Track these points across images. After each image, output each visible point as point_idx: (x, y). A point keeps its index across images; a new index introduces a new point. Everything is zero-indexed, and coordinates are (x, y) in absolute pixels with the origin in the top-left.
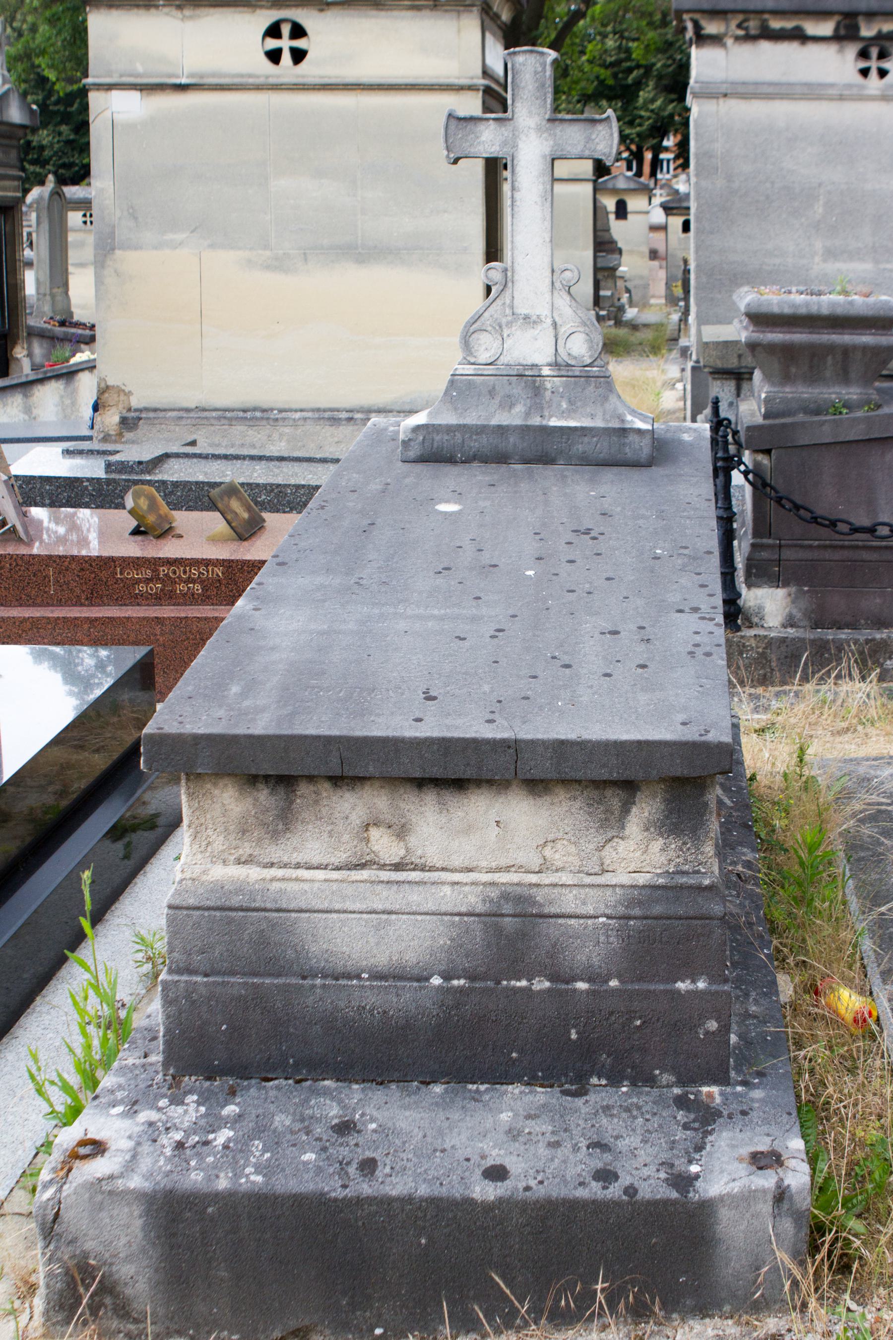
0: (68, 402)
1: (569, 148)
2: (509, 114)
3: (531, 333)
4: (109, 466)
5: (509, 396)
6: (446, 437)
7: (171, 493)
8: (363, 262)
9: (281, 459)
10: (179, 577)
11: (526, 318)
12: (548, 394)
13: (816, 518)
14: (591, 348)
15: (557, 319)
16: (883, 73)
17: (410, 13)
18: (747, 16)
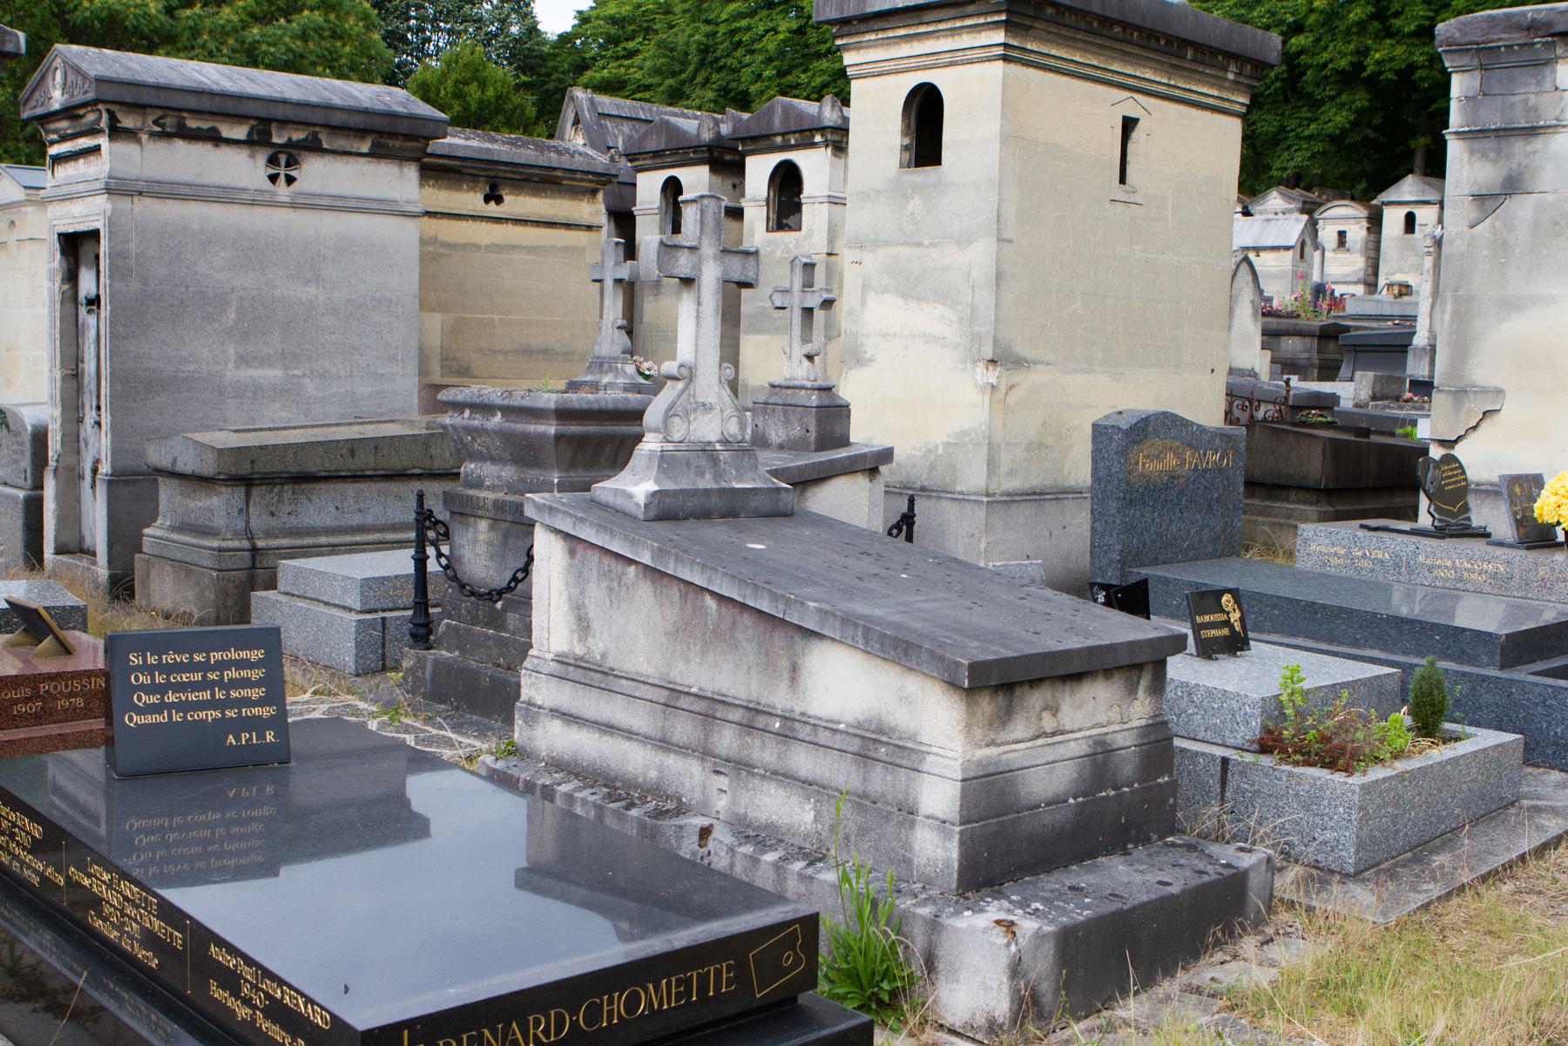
16: (290, 180)
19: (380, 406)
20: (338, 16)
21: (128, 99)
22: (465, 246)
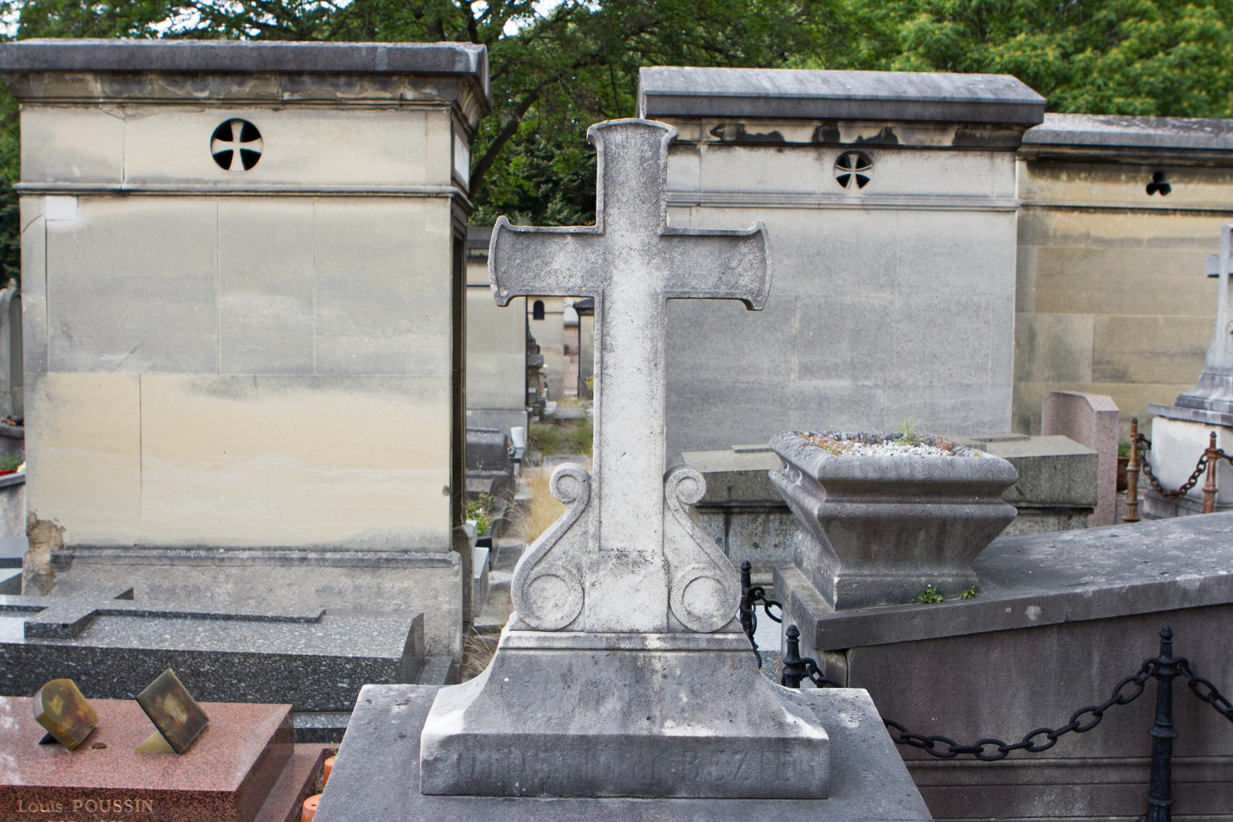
0: (11, 515)
1: (694, 282)
2: (598, 226)
3: (629, 580)
4: (29, 629)
5: (594, 684)
6: (496, 756)
7: (101, 662)
8: (319, 386)
9: (228, 618)
10: (98, 812)
11: (622, 555)
12: (657, 680)
13: (908, 737)
14: (723, 603)
15: (670, 557)
16: (862, 181)
17: (373, 113)
18: (723, 121)
19: (964, 419)
20: (1216, 46)
21: (680, 111)
22: (1122, 242)
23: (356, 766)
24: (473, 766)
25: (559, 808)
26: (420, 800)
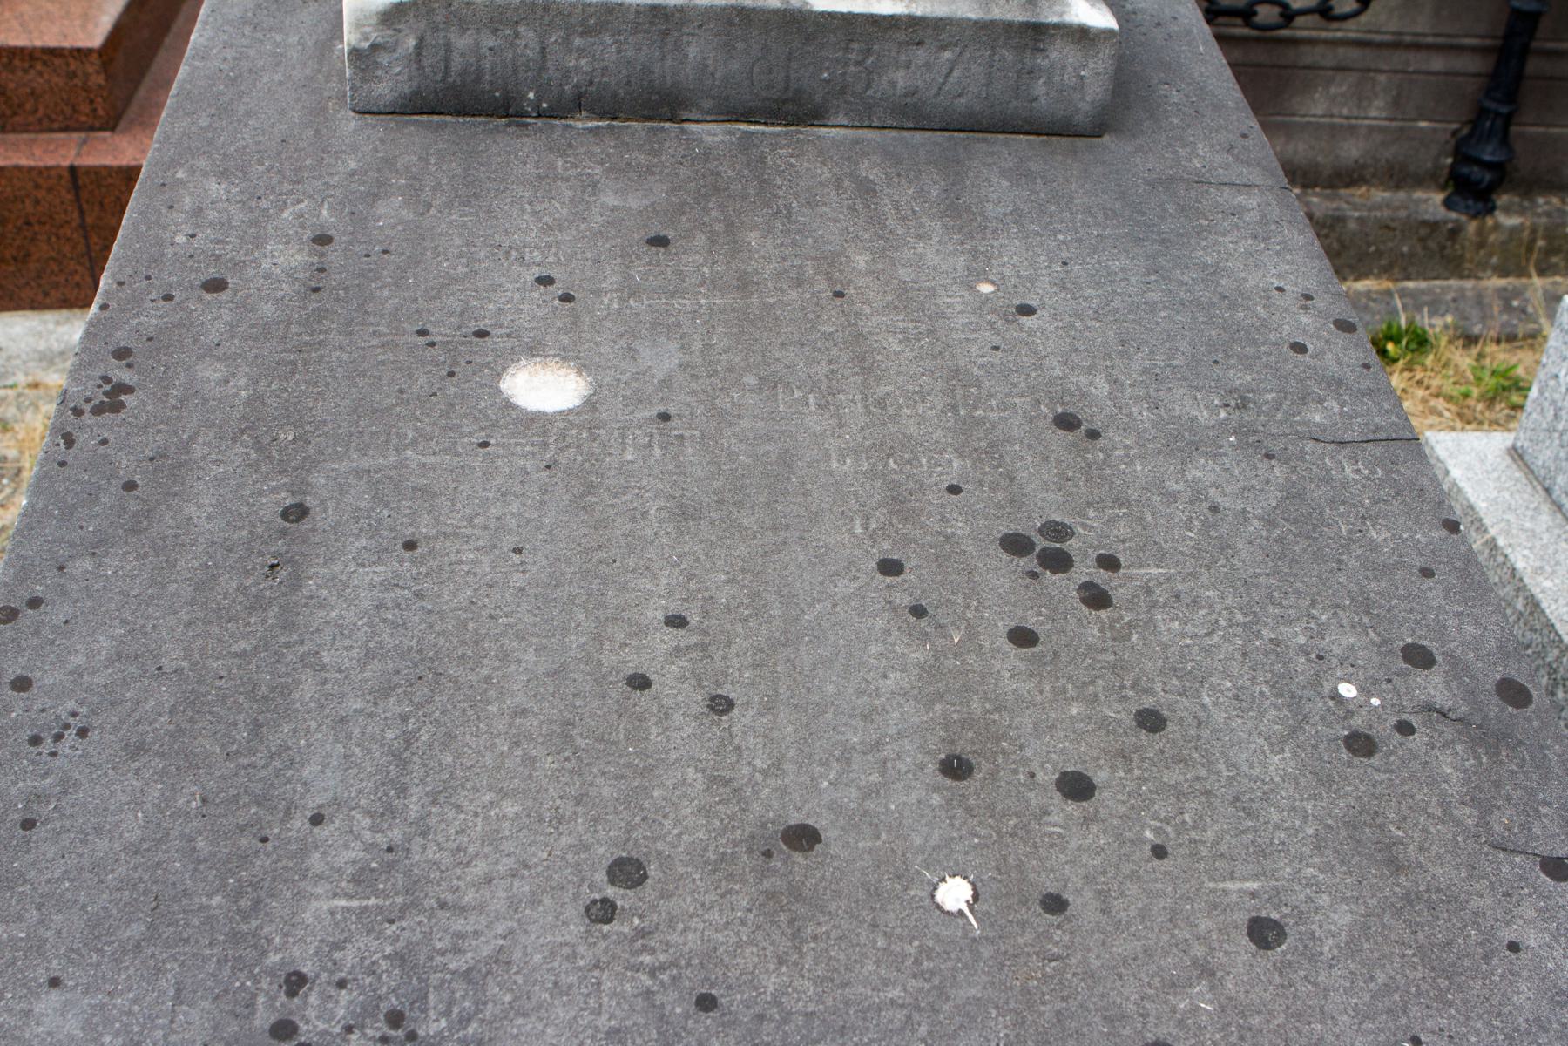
23: (230, 53)
24: (447, 60)
25: (610, 141)
26: (349, 124)
